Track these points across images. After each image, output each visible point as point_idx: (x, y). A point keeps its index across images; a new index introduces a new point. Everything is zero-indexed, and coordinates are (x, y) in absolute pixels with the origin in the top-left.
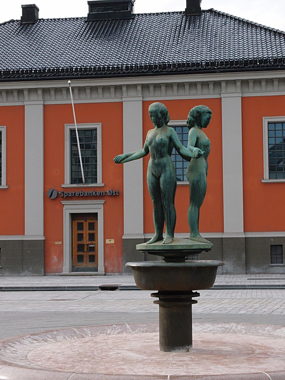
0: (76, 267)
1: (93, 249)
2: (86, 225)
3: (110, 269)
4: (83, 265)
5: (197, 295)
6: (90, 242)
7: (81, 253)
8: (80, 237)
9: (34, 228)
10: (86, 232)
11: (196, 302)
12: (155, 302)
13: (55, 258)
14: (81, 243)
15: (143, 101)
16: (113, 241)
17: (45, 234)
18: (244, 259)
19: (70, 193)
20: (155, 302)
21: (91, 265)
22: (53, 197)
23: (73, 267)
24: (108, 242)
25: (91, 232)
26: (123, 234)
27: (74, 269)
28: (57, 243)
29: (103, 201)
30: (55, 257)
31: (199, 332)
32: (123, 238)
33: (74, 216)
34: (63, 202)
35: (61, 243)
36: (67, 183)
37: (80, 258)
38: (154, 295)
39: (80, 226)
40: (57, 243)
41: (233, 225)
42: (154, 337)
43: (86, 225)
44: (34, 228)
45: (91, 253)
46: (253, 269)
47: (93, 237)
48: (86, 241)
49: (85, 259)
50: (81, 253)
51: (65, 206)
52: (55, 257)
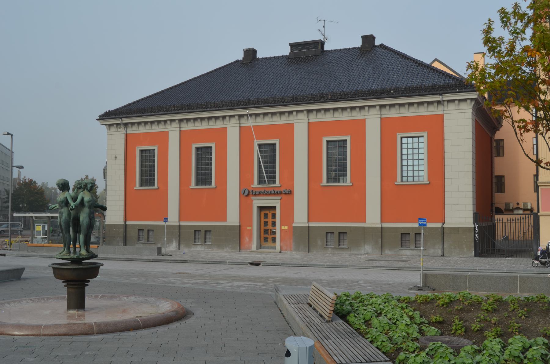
0: (263, 246)
1: (274, 233)
2: (270, 215)
3: (284, 248)
4: (267, 244)
5: (89, 281)
6: (272, 228)
7: (266, 236)
8: (266, 223)
9: (233, 218)
10: (270, 220)
11: (87, 285)
12: (65, 286)
13: (247, 239)
14: (266, 228)
15: (308, 122)
16: (286, 228)
17: (239, 222)
18: (380, 243)
19: (257, 191)
20: (65, 286)
21: (272, 244)
22: (247, 194)
23: (261, 245)
24: (283, 228)
25: (273, 220)
26: (293, 222)
27: (260, 247)
28: (248, 228)
29: (279, 198)
30: (247, 238)
31: (88, 302)
32: (294, 225)
33: (261, 208)
34: (253, 198)
35: (250, 228)
36: (255, 184)
37: (266, 240)
38: (64, 282)
39: (266, 216)
40: (248, 228)
41: (373, 217)
42: (65, 303)
43: (270, 215)
44: (233, 218)
45: (273, 236)
46: (387, 252)
47: (274, 224)
48: (269, 227)
49: (269, 240)
50: (266, 236)
51: (254, 201)
52: (247, 238)
